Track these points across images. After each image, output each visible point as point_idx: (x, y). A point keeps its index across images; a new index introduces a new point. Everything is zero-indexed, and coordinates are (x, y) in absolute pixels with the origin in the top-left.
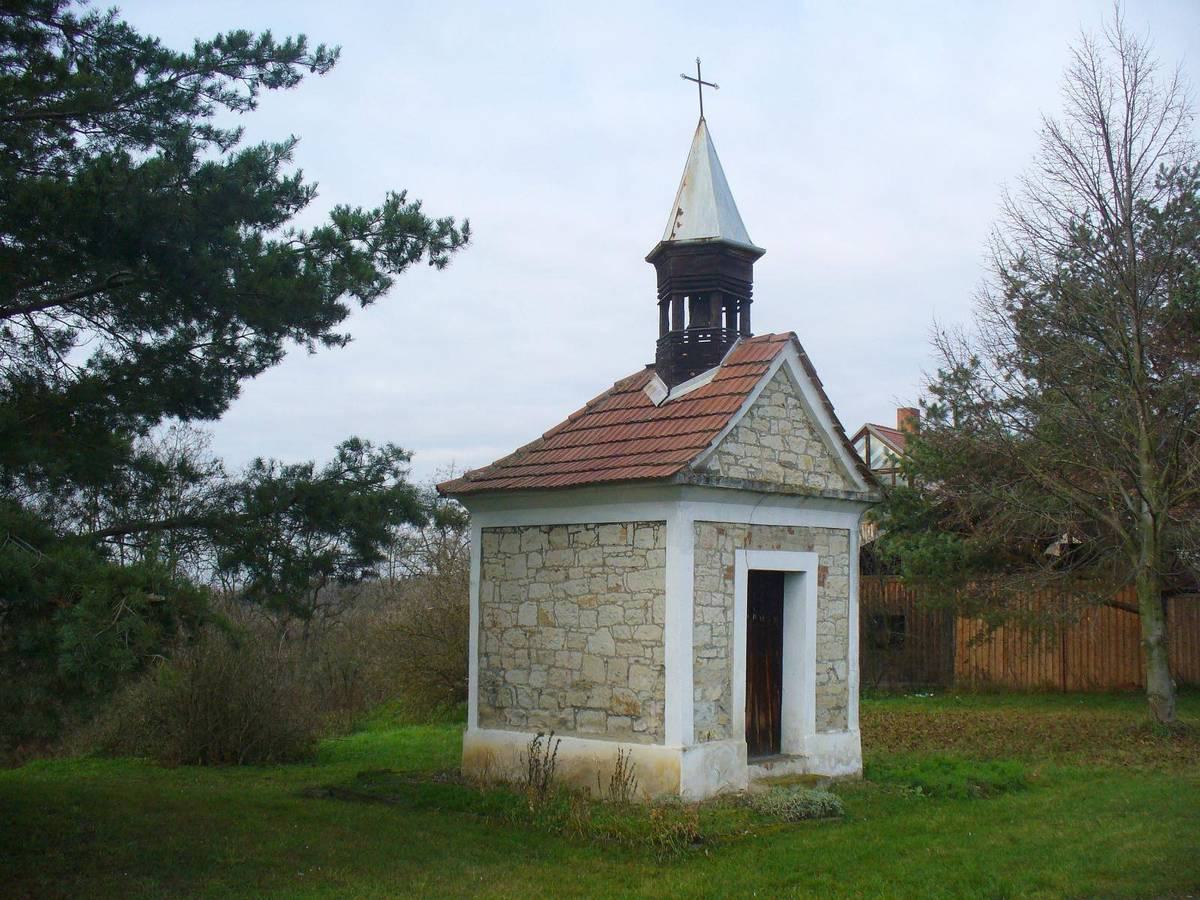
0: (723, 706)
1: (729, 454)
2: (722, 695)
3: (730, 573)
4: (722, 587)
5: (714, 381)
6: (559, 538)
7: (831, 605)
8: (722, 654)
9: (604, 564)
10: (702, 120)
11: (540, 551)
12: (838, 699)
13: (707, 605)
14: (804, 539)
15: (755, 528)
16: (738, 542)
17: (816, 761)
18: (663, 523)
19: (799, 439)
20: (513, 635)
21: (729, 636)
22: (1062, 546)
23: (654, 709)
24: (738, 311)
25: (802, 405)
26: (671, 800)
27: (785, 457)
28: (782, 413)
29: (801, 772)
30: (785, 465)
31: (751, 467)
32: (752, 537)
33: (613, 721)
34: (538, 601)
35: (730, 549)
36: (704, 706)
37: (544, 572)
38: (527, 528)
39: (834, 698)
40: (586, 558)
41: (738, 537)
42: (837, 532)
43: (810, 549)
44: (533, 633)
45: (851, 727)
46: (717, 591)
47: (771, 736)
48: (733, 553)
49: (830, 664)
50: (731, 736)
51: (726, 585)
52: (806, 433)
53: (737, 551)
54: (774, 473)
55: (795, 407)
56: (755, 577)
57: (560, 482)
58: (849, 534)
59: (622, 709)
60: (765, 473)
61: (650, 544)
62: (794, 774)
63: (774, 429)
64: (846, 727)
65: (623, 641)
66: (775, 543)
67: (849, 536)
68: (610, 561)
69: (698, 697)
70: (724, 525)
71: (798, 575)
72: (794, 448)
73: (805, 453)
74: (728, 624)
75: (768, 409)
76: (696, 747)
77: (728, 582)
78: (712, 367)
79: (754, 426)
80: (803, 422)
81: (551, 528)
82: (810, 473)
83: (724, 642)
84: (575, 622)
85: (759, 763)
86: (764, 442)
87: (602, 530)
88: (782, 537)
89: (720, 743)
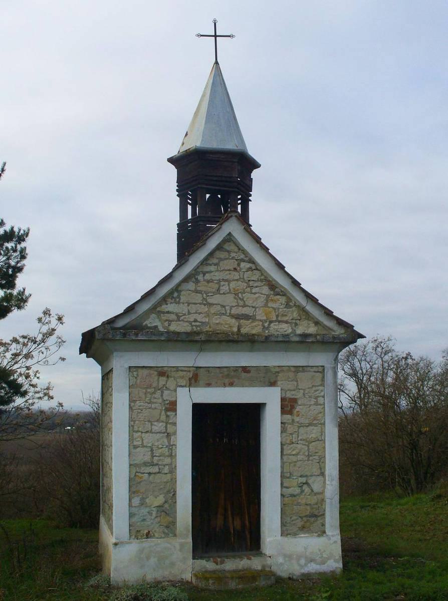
0: (167, 510)
1: (168, 312)
2: (166, 502)
3: (172, 406)
4: (163, 417)
8: (166, 470)
10: (217, 63)
12: (312, 508)
13: (147, 432)
14: (268, 378)
15: (202, 369)
17: (281, 560)
19: (257, 295)
21: (172, 456)
24: (239, 204)
25: (255, 267)
26: (203, 570)
28: (236, 275)
29: (259, 568)
30: (238, 317)
31: (195, 321)
32: (195, 378)
39: (308, 508)
41: (182, 377)
42: (309, 369)
43: (273, 384)
45: (328, 532)
46: (158, 421)
47: (248, 536)
48: (175, 391)
49: (304, 480)
50: (175, 535)
51: (167, 416)
52: (266, 290)
53: (179, 389)
58: (324, 370)
60: (212, 325)
62: (250, 569)
63: (224, 288)
64: (324, 532)
66: (227, 381)
67: (323, 372)
70: (165, 369)
72: (249, 303)
73: (266, 305)
74: (171, 447)
75: (216, 274)
76: (131, 543)
79: (199, 289)
80: (261, 281)
82: (271, 322)
83: (168, 460)
85: (202, 558)
86: (210, 300)
88: (231, 376)
89: (159, 541)
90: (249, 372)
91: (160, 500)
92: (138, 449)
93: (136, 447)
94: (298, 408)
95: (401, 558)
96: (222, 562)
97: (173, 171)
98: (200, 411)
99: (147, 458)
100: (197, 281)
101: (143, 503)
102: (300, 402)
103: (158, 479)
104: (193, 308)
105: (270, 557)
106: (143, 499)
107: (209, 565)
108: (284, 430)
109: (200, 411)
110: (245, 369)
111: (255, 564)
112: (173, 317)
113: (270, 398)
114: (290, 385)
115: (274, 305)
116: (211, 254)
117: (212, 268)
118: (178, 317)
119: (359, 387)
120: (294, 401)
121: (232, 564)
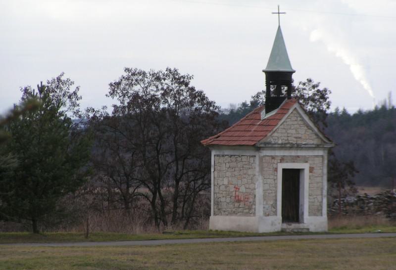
0: (274, 206)
3: (276, 170)
5: (276, 114)
6: (233, 159)
7: (315, 178)
8: (274, 192)
9: (243, 167)
10: (279, 27)
11: (229, 162)
14: (305, 160)
16: (279, 161)
18: (255, 156)
20: (222, 188)
22: (135, 171)
23: (254, 207)
27: (297, 136)
28: (296, 122)
30: (296, 138)
32: (282, 160)
33: (245, 211)
34: (228, 177)
35: (276, 163)
36: (267, 206)
37: (230, 169)
38: (226, 155)
40: (240, 165)
43: (307, 162)
44: (227, 186)
52: (306, 128)
54: (293, 140)
55: (300, 120)
56: (285, 171)
57: (235, 144)
59: (247, 207)
61: (252, 162)
63: (292, 128)
65: (247, 188)
68: (244, 166)
69: (265, 204)
71: (303, 169)
73: (305, 134)
74: (276, 184)
77: (276, 172)
78: (276, 109)
81: (231, 156)
84: (236, 183)
87: (243, 157)
88: (295, 159)
91: (271, 203)
94: (315, 171)
96: (291, 225)
97: (264, 75)
98: (284, 170)
99: (268, 187)
100: (284, 125)
101: (267, 204)
102: (315, 168)
107: (285, 226)
108: (310, 178)
109: (284, 170)
110: (298, 157)
112: (277, 138)
116: (301, 117)
117: (289, 120)
118: (278, 137)
119: (285, 234)
120: (313, 168)
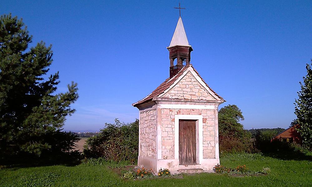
3: (173, 120)
4: (171, 123)
21: (173, 134)
28: (190, 83)
32: (179, 112)
43: (200, 114)
90: (194, 110)
92: (164, 132)
93: (163, 132)
95: (24, 49)
102: (207, 120)
103: (170, 141)
104: (179, 92)
105: (42, 42)
106: (165, 147)
107: (183, 167)
110: (193, 110)
111: (197, 167)
113: (200, 118)
114: (205, 115)
115: (201, 92)
121: (190, 167)
